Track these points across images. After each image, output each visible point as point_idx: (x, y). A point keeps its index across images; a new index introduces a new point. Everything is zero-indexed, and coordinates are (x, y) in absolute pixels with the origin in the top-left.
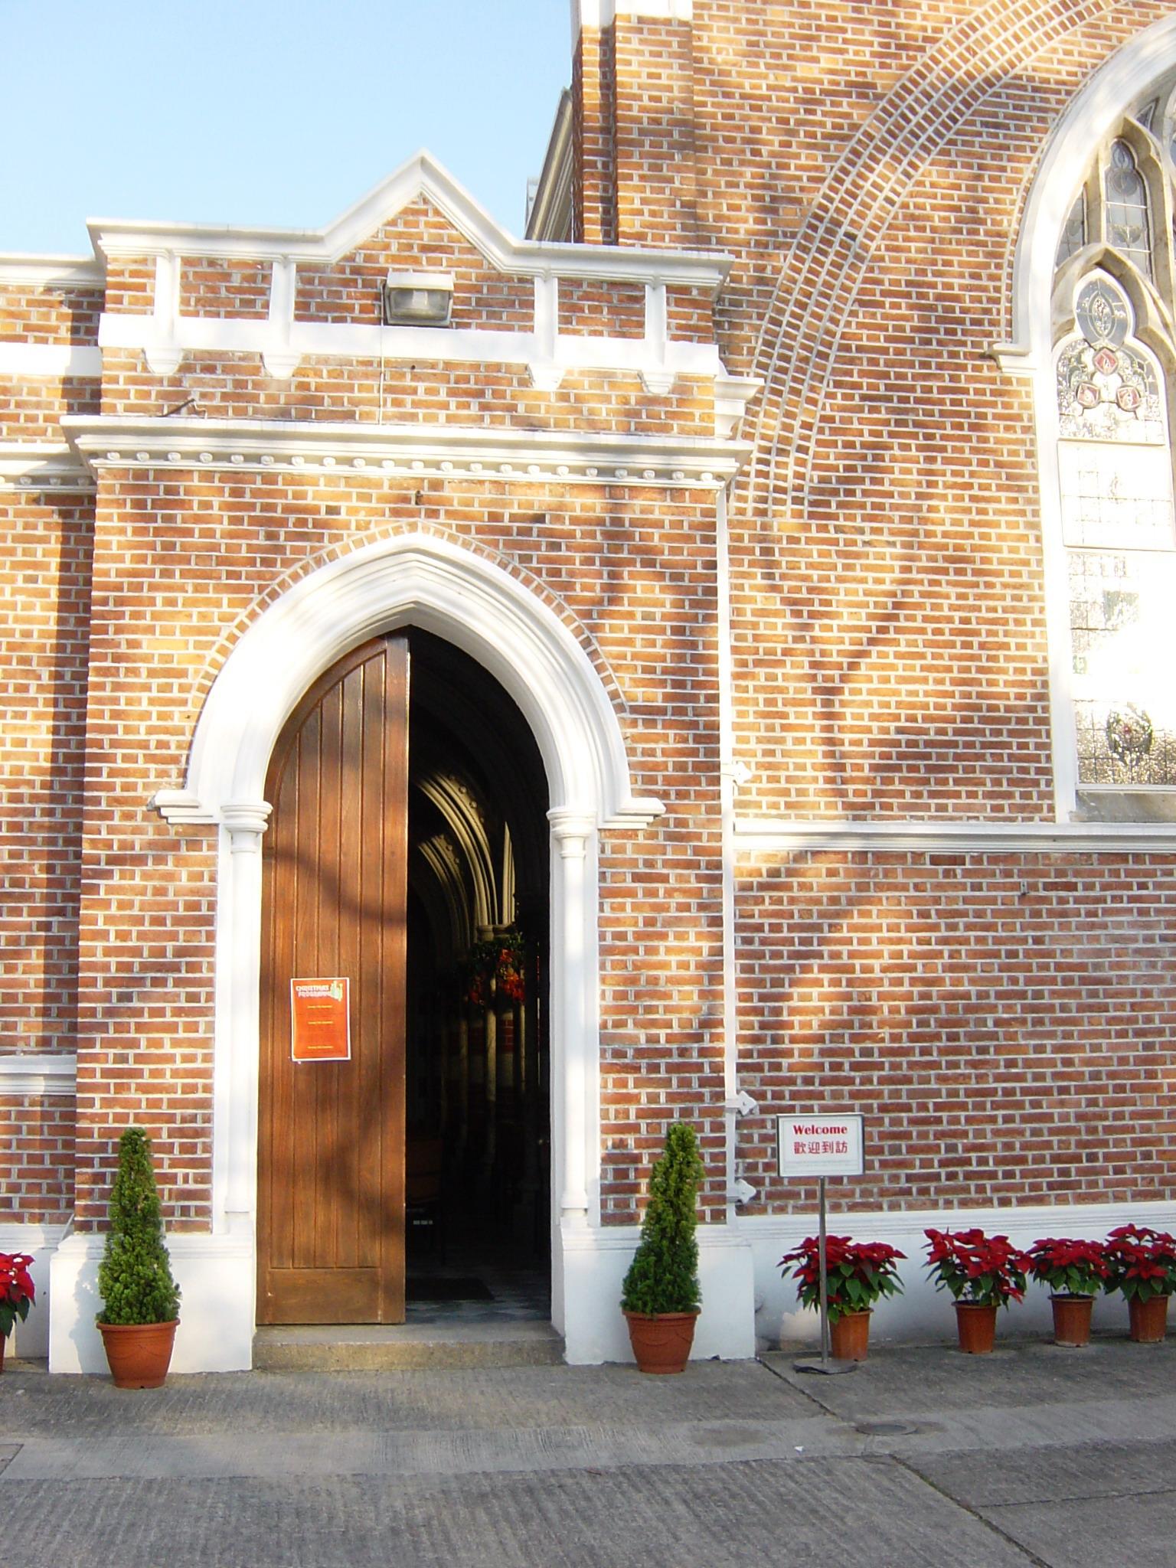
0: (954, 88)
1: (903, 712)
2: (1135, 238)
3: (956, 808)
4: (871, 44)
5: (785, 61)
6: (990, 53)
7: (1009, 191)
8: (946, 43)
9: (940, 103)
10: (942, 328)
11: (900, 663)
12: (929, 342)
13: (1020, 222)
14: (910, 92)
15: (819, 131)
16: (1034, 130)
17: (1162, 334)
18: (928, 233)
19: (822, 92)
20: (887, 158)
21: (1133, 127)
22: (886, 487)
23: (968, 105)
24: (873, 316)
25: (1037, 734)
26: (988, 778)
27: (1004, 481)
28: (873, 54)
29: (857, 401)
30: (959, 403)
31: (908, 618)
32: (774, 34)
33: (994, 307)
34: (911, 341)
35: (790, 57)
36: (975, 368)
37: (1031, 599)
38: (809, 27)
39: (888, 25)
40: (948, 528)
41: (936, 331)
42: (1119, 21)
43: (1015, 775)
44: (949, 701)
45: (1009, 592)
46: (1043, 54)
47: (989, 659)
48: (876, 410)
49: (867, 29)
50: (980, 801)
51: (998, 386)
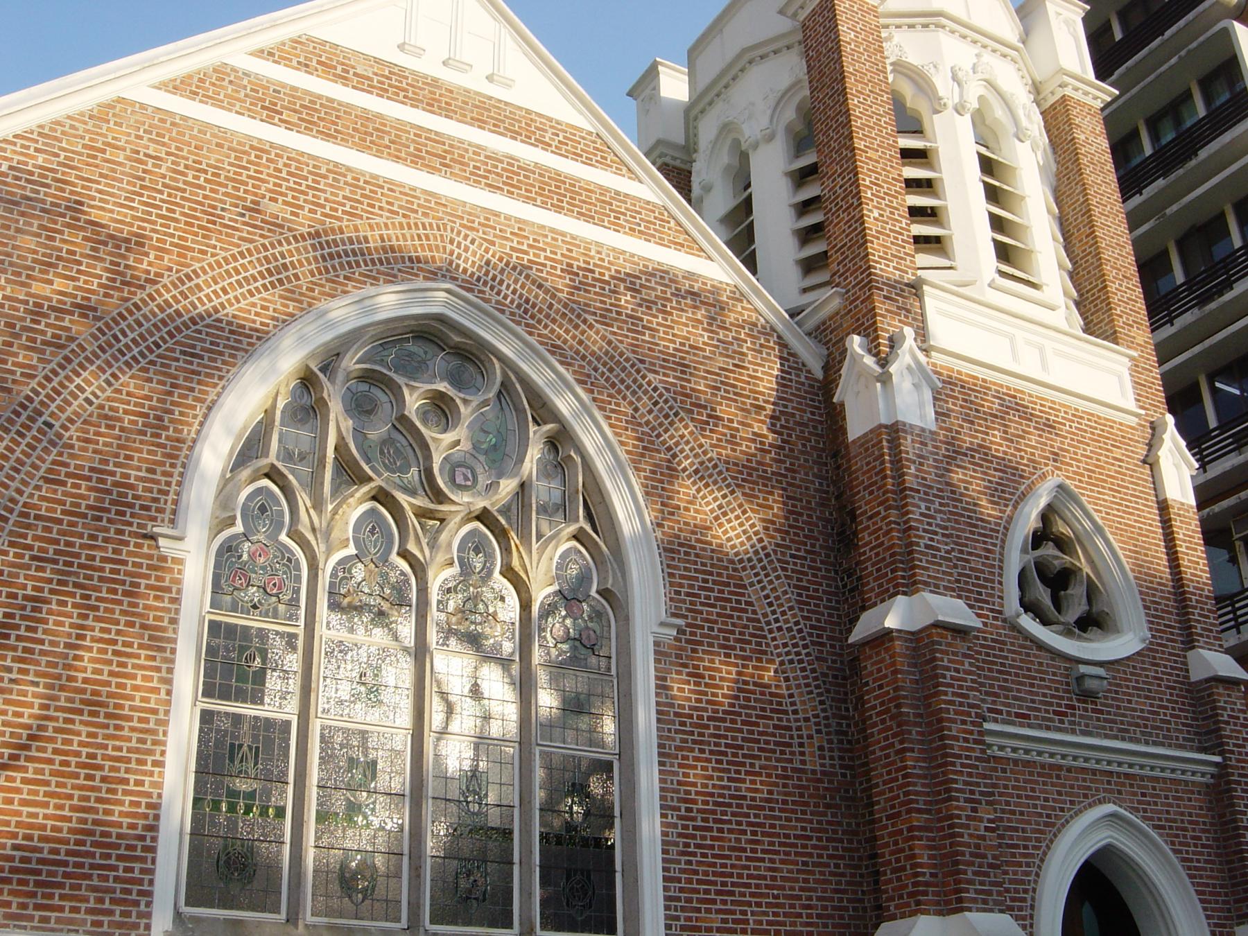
0: (163, 321)
1: (21, 831)
2: (302, 458)
3: (58, 920)
4: (100, 277)
5: (23, 279)
6: (199, 299)
7: (194, 408)
8: (165, 286)
9: (149, 331)
10: (114, 508)
11: (26, 787)
12: (100, 519)
13: (198, 432)
14: (124, 319)
15: (39, 337)
16: (224, 362)
17: (310, 537)
18: (117, 432)
19: (50, 307)
20: (93, 368)
21: (312, 372)
22: (39, 635)
23: (172, 336)
24: (55, 491)
25: (143, 860)
26: (92, 896)
27: (146, 641)
28: (100, 285)
29: (26, 560)
30: (118, 572)
31: (39, 749)
32: (19, 257)
33: (163, 497)
34: (85, 516)
35: (28, 276)
36: (137, 545)
37: (155, 743)
38: (50, 256)
39: (118, 265)
40: (89, 675)
41: (108, 511)
42: (313, 290)
43: (118, 895)
44: (65, 825)
45: (135, 735)
46: (245, 304)
47: (109, 791)
48: (42, 569)
49: (100, 265)
50: (81, 916)
51: (155, 562)
